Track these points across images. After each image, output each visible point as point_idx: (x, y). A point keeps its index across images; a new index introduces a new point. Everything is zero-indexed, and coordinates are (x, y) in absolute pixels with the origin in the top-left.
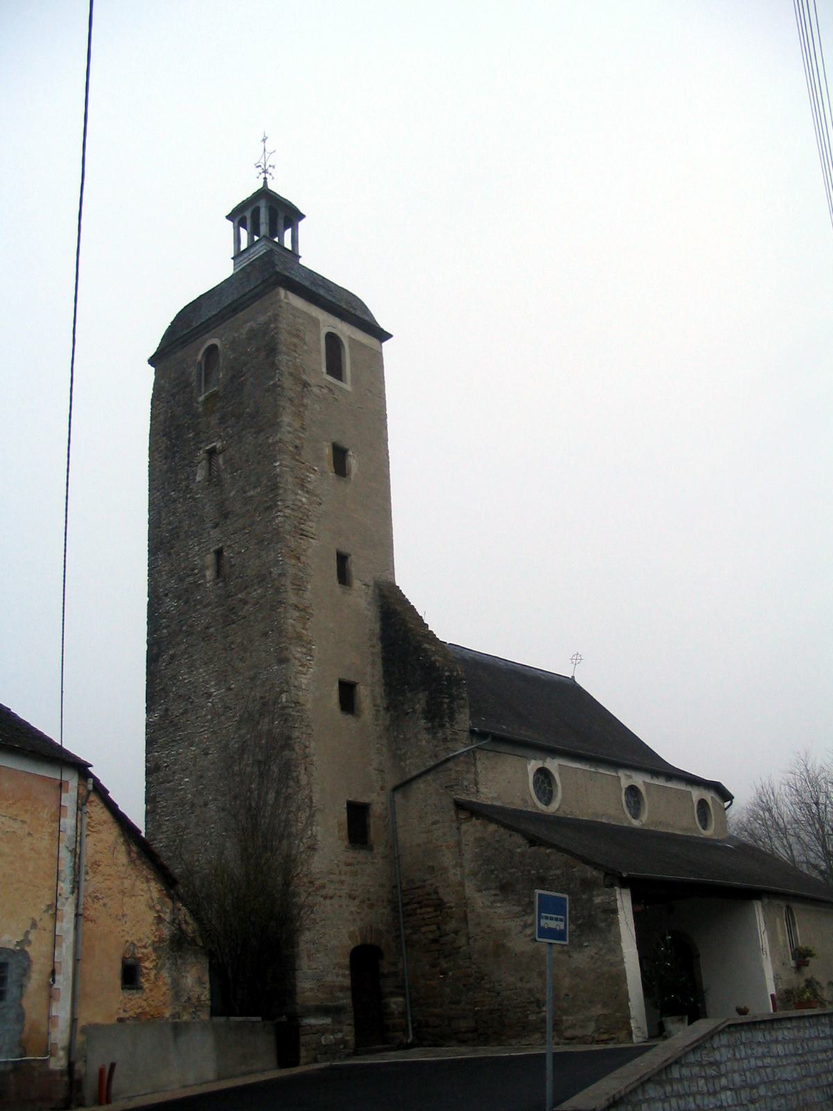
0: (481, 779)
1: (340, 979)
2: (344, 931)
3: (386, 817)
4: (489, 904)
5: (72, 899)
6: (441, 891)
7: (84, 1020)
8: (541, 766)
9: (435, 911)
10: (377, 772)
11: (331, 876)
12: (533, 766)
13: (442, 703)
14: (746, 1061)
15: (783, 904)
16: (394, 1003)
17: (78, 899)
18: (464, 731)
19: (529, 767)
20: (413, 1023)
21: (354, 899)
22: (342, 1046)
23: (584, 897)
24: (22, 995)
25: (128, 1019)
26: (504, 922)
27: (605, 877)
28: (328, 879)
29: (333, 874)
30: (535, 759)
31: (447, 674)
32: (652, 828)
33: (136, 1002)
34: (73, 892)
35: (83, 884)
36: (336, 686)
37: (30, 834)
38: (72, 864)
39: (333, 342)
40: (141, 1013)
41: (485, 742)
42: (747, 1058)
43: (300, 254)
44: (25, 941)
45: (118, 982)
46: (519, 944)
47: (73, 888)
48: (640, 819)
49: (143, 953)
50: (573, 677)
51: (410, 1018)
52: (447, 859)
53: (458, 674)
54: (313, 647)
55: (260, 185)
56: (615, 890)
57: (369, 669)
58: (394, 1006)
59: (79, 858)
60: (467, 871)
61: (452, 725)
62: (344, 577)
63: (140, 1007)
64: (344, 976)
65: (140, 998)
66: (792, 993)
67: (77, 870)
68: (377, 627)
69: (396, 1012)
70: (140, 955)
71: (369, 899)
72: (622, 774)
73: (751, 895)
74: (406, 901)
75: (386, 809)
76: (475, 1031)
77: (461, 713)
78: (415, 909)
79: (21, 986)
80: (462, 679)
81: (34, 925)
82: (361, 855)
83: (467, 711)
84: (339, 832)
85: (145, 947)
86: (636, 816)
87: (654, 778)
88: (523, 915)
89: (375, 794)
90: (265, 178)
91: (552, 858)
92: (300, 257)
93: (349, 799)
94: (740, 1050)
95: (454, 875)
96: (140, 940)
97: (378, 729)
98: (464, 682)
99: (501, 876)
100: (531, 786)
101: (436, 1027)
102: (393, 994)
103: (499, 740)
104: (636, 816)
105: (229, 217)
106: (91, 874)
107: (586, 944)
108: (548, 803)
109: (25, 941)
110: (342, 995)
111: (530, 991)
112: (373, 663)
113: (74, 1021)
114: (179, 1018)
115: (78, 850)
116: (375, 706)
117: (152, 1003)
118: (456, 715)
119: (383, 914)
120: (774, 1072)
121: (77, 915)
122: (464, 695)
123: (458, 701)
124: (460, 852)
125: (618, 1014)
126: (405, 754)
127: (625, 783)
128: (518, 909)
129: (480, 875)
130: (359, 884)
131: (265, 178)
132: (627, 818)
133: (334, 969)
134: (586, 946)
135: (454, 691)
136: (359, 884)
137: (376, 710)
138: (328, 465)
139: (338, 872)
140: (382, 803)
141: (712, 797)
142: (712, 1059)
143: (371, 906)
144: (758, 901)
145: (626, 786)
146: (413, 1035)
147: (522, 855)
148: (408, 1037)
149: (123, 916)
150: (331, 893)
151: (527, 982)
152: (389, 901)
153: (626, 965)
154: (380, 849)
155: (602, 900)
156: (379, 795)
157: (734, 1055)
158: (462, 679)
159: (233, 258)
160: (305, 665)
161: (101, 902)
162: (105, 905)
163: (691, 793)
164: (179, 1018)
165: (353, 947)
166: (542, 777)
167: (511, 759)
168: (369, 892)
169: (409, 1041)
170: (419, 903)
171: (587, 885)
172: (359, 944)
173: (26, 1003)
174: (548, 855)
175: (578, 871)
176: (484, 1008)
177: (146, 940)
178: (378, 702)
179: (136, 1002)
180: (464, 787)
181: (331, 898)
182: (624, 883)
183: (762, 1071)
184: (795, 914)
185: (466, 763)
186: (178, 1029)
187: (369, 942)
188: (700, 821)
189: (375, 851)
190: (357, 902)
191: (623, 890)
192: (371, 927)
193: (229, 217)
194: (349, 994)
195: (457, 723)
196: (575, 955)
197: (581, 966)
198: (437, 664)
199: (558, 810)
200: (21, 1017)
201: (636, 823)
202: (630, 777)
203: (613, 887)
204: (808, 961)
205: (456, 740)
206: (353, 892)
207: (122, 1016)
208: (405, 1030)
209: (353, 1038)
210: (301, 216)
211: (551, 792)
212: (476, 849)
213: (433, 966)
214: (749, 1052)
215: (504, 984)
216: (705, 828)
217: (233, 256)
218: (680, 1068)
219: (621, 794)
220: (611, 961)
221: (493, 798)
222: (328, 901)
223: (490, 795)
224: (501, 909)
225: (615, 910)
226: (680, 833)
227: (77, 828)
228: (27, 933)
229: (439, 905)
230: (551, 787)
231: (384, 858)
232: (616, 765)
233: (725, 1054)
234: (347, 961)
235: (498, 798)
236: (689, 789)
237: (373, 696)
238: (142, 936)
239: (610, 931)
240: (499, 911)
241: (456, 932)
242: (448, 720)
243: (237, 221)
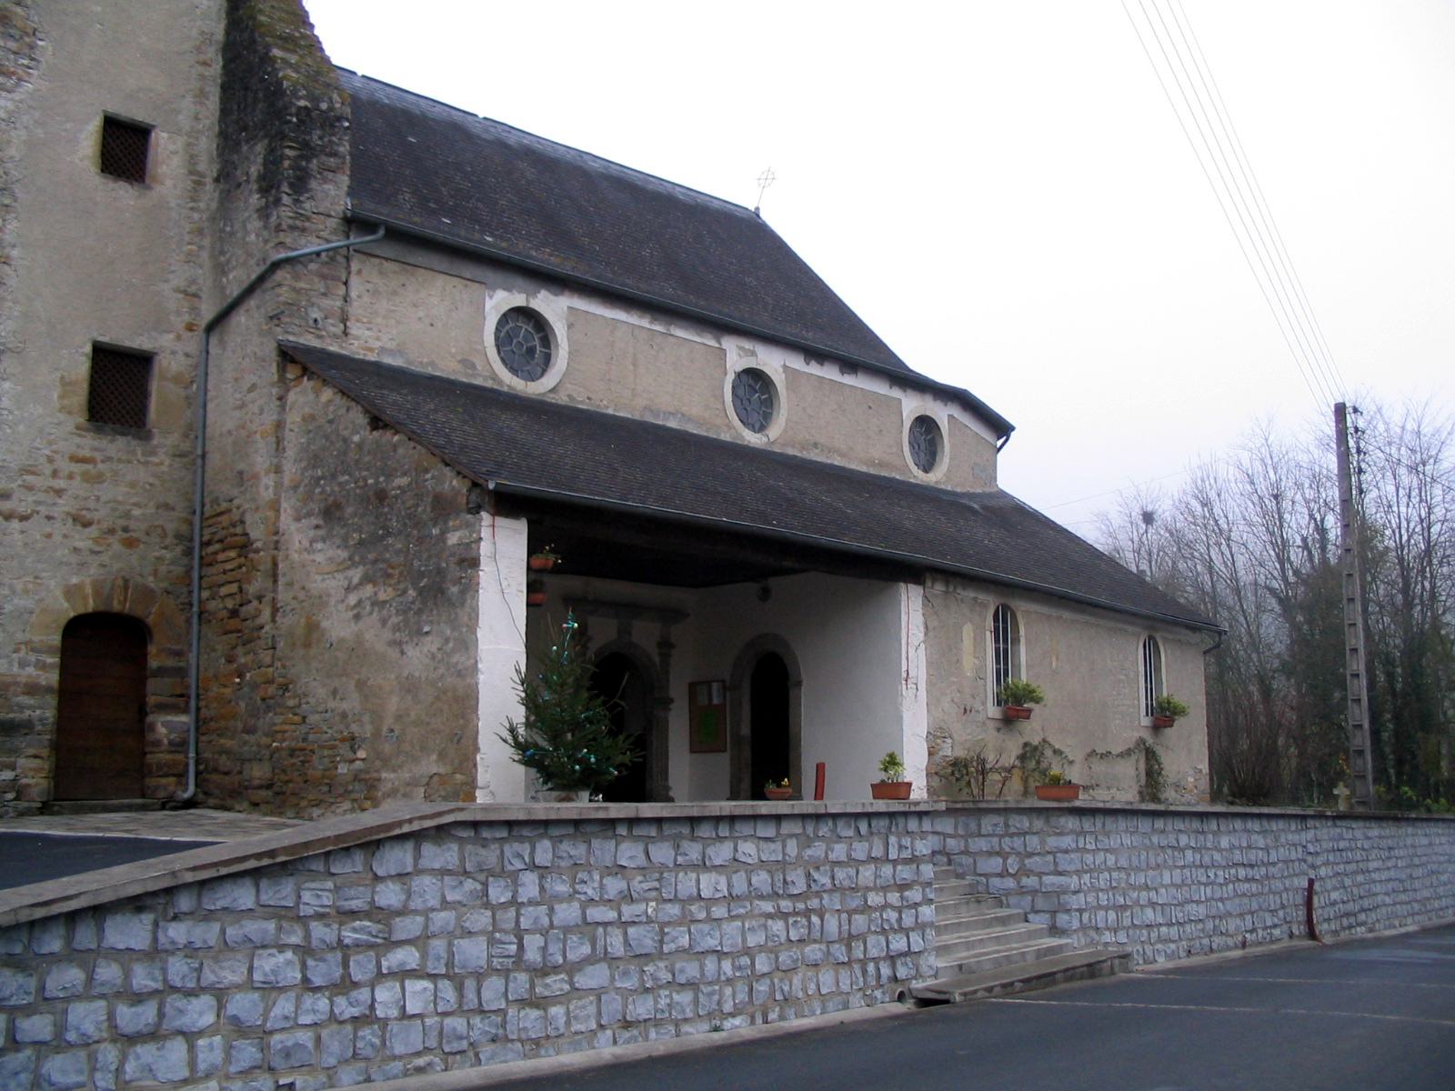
0: (355, 309)
1: (30, 670)
2: (53, 583)
3: (192, 382)
4: (306, 543)
6: (248, 519)
9: (240, 556)
10: (181, 296)
11: (29, 478)
13: (282, 157)
15: (991, 602)
16: (163, 724)
18: (329, 216)
19: (489, 304)
20: (197, 763)
21: (86, 524)
22: (10, 796)
23: (434, 531)
26: (323, 580)
27: (470, 491)
28: (20, 482)
29: (33, 473)
31: (302, 103)
32: (790, 451)
36: (95, 125)
46: (337, 625)
48: (767, 432)
50: (757, 209)
51: (192, 755)
52: (261, 459)
53: (331, 109)
54: (40, 43)
56: (481, 520)
57: (187, 105)
58: (163, 730)
60: (287, 481)
61: (297, 201)
64: (42, 666)
66: (966, 766)
68: (218, 29)
69: (166, 741)
71: (126, 529)
72: (731, 345)
74: (206, 538)
75: (196, 367)
76: (269, 787)
77: (325, 180)
78: (216, 553)
80: (339, 119)
82: (116, 446)
83: (344, 180)
84: (61, 397)
87: (813, 363)
88: (348, 568)
89: (171, 336)
91: (401, 451)
93: (101, 339)
95: (266, 487)
97: (196, 216)
98: (347, 124)
99: (328, 489)
101: (226, 774)
102: (163, 708)
103: (402, 237)
104: (761, 428)
107: (426, 629)
110: (32, 702)
111: (344, 715)
112: (202, 95)
116: (191, 173)
118: (313, 184)
119: (160, 559)
122: (341, 149)
123: (324, 158)
124: (278, 443)
125: (458, 776)
126: (228, 261)
128: (343, 554)
129: (301, 489)
130: (104, 498)
132: (730, 426)
133: (17, 651)
134: (427, 633)
135: (315, 137)
136: (104, 498)
137: (194, 182)
139: (48, 471)
140: (187, 355)
141: (951, 417)
143: (130, 543)
144: (911, 586)
145: (739, 368)
146: (197, 785)
147: (360, 446)
148: (186, 790)
150: (22, 509)
151: (342, 699)
152: (179, 537)
153: (481, 677)
154: (166, 439)
155: (460, 538)
156: (179, 338)
158: (339, 119)
160: (13, 73)
163: (900, 401)
165: (72, 614)
167: (441, 280)
168: (127, 515)
169: (186, 795)
170: (221, 541)
171: (443, 508)
172: (90, 610)
174: (395, 447)
175: (433, 478)
176: (284, 745)
178: (202, 167)
180: (311, 322)
181: (24, 518)
182: (507, 504)
185: (324, 277)
187: (116, 607)
189: (155, 442)
190: (93, 531)
191: (500, 521)
192: (126, 581)
194: (52, 701)
195: (312, 198)
196: (411, 652)
197: (417, 674)
198: (285, 84)
199: (553, 390)
201: (752, 439)
202: (753, 354)
203: (478, 513)
204: (1030, 711)
205: (304, 230)
206: (84, 512)
208: (181, 776)
209: (44, 784)
212: (302, 437)
213: (230, 660)
215: (312, 700)
218: (156, 924)
220: (460, 667)
221: (383, 350)
222: (15, 524)
223: (377, 344)
224: (326, 553)
225: (473, 559)
226: (864, 469)
229: (245, 546)
230: (550, 349)
231: (175, 455)
232: (722, 328)
234: (56, 639)
235: (399, 352)
236: (896, 393)
237: (192, 156)
239: (463, 604)
240: (319, 558)
241: (260, 598)
242: (287, 190)
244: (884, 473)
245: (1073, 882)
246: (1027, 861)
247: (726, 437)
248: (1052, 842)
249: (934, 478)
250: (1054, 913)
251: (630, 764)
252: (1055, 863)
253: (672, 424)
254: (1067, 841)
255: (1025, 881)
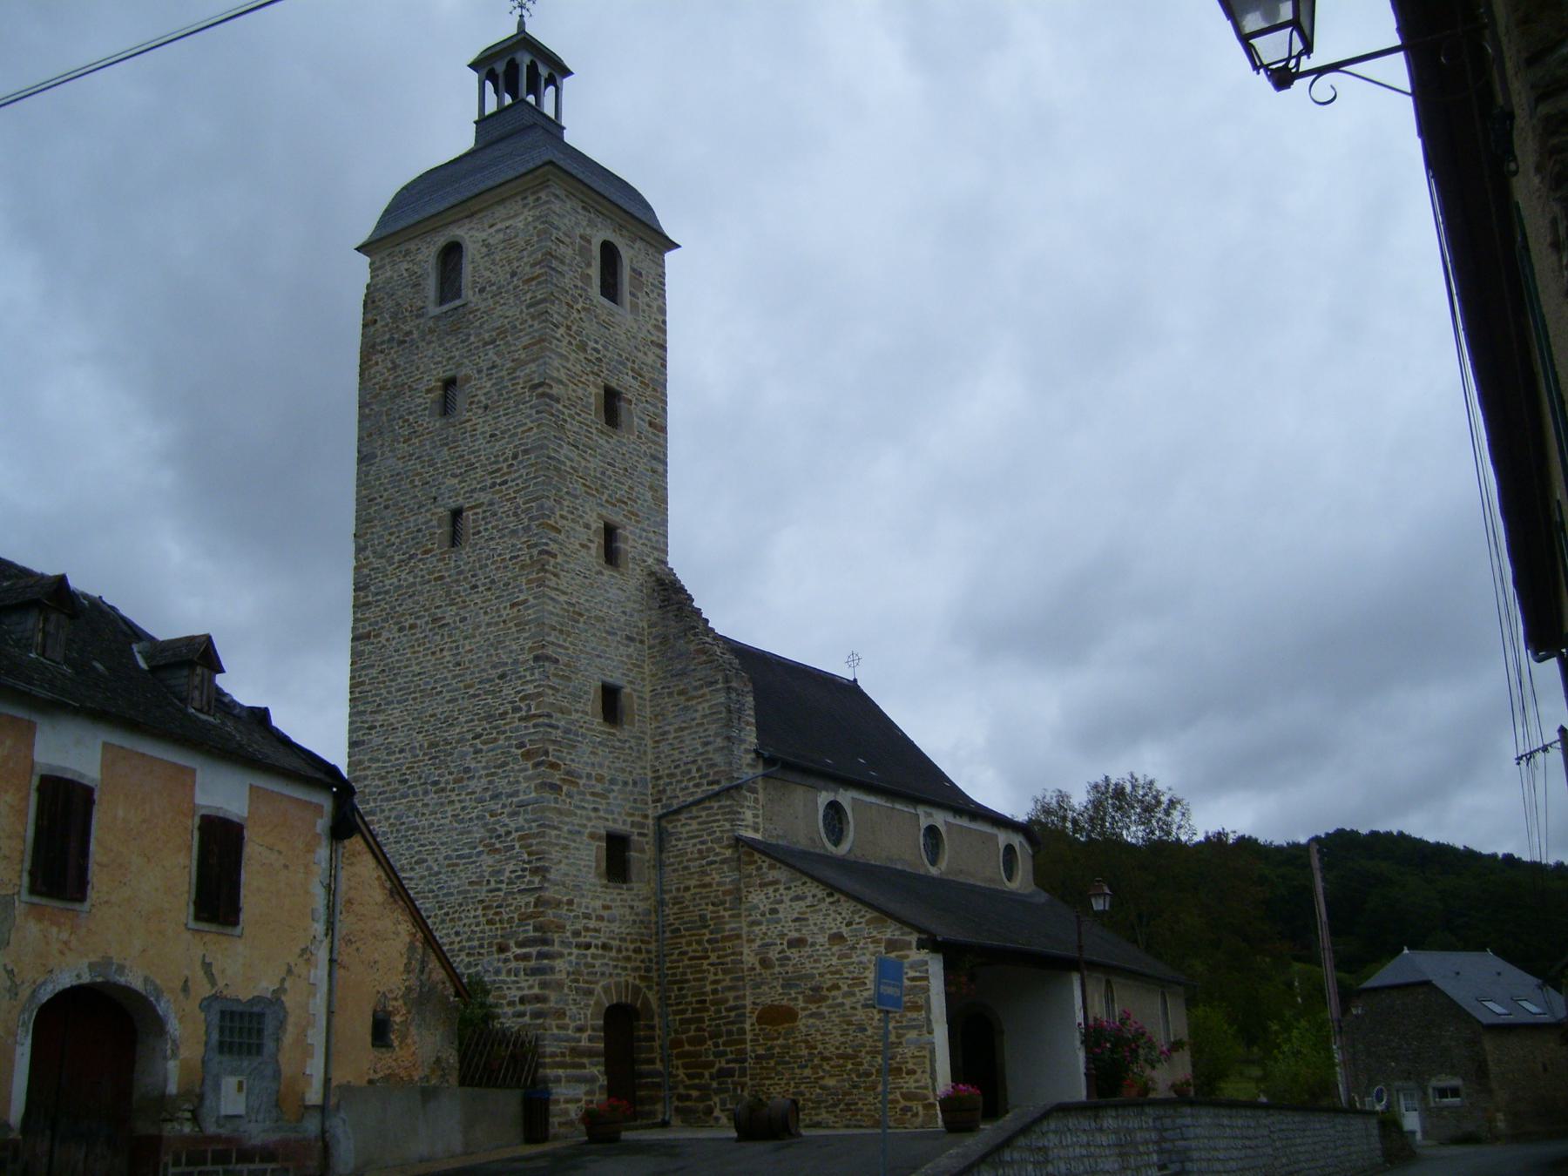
5: (326, 942)
7: (339, 1077)
8: (832, 799)
12: (824, 798)
14: (1071, 1149)
17: (332, 942)
24: (278, 1050)
25: (378, 1080)
30: (827, 791)
32: (951, 877)
33: (387, 1061)
34: (326, 935)
35: (338, 925)
37: (286, 867)
38: (326, 902)
39: (610, 254)
40: (390, 1074)
41: (774, 769)
42: (1073, 1145)
43: (563, 124)
44: (281, 990)
45: (369, 1039)
47: (327, 929)
49: (393, 1006)
50: (855, 680)
55: (512, 30)
59: (334, 896)
62: (611, 555)
63: (390, 1067)
65: (391, 1057)
67: (331, 909)
70: (390, 1009)
73: (1067, 965)
79: (278, 1040)
81: (290, 971)
85: (396, 999)
86: (933, 862)
90: (521, 16)
92: (563, 128)
94: (1066, 1138)
96: (391, 991)
100: (822, 831)
105: (474, 66)
106: (344, 913)
108: (837, 843)
109: (281, 990)
113: (327, 1081)
114: (427, 1081)
115: (333, 886)
117: (402, 1064)
120: (1096, 1162)
121: (332, 961)
127: (924, 823)
131: (521, 16)
132: (923, 864)
138: (595, 417)
141: (1020, 842)
142: (1040, 1145)
149: (375, 962)
157: (1061, 1142)
159: (475, 122)
161: (354, 946)
162: (358, 949)
163: (997, 836)
164: (427, 1081)
166: (832, 812)
173: (282, 1059)
177: (397, 991)
179: (387, 1061)
183: (1085, 1160)
184: (1114, 988)
186: (428, 1094)
188: (1005, 871)
193: (474, 66)
200: (277, 1074)
201: (934, 871)
202: (930, 815)
207: (371, 1077)
210: (567, 72)
211: (841, 830)
214: (1075, 1139)
216: (1009, 879)
217: (477, 118)
219: (918, 836)
227: (331, 859)
228: (283, 980)
232: (915, 800)
233: (1052, 1140)
236: (994, 831)
238: (393, 987)
243: (485, 71)
244: (993, 886)
245: (1193, 1144)
246: (1164, 1134)
247: (922, 872)
248: (1179, 1121)
249: (843, 849)
250: (1182, 1162)
251: (1174, 1095)
252: (1182, 1134)
253: (899, 867)
254: (1188, 1121)
255: (1164, 1145)
